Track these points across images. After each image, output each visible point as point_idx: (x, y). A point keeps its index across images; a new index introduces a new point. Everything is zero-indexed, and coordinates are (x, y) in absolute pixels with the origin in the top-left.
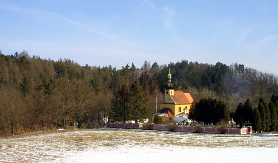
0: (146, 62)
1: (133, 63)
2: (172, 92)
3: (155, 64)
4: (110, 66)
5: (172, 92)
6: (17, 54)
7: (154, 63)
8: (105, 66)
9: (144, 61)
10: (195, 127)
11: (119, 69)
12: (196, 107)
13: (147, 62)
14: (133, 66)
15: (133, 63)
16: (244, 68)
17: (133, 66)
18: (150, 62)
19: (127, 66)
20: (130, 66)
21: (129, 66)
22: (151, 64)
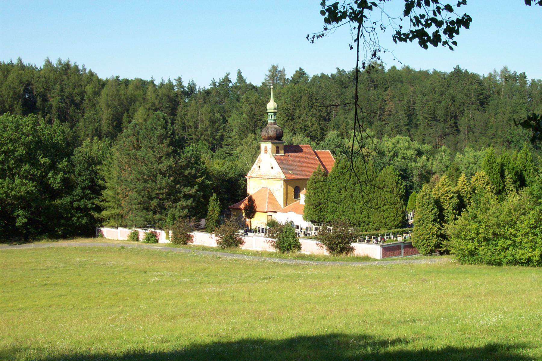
0: (274, 68)
1: (239, 73)
2: (266, 148)
3: (301, 74)
4: (179, 80)
5: (266, 148)
6: (214, 83)
7: (297, 72)
8: (166, 81)
9: (270, 67)
10: (415, 179)
11: (202, 87)
12: (124, 355)
13: (279, 69)
14: (240, 78)
15: (239, 73)
16: (525, 83)
17: (240, 78)
18: (284, 70)
19: (227, 80)
20: (234, 79)
21: (230, 81)
22: (289, 75)
